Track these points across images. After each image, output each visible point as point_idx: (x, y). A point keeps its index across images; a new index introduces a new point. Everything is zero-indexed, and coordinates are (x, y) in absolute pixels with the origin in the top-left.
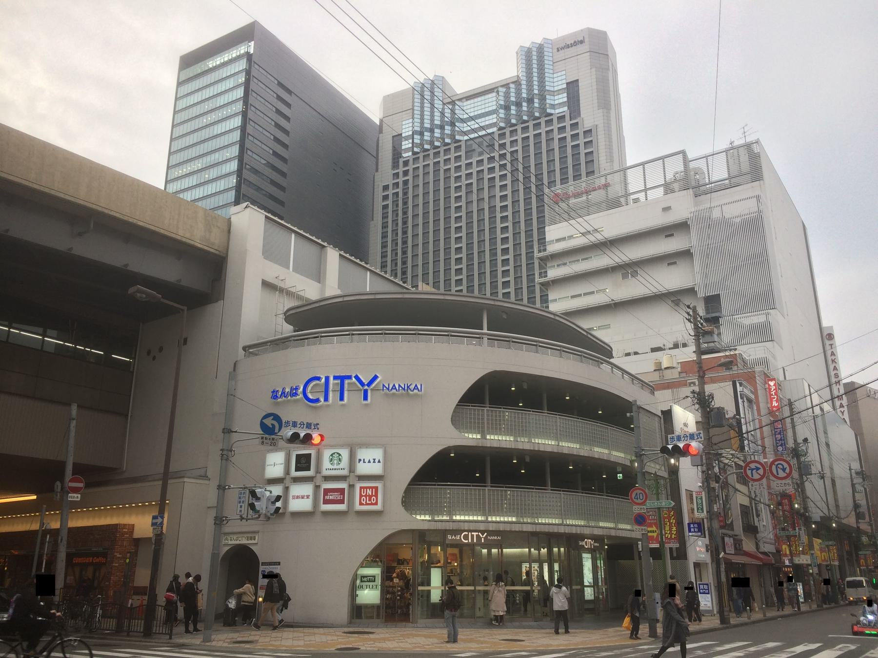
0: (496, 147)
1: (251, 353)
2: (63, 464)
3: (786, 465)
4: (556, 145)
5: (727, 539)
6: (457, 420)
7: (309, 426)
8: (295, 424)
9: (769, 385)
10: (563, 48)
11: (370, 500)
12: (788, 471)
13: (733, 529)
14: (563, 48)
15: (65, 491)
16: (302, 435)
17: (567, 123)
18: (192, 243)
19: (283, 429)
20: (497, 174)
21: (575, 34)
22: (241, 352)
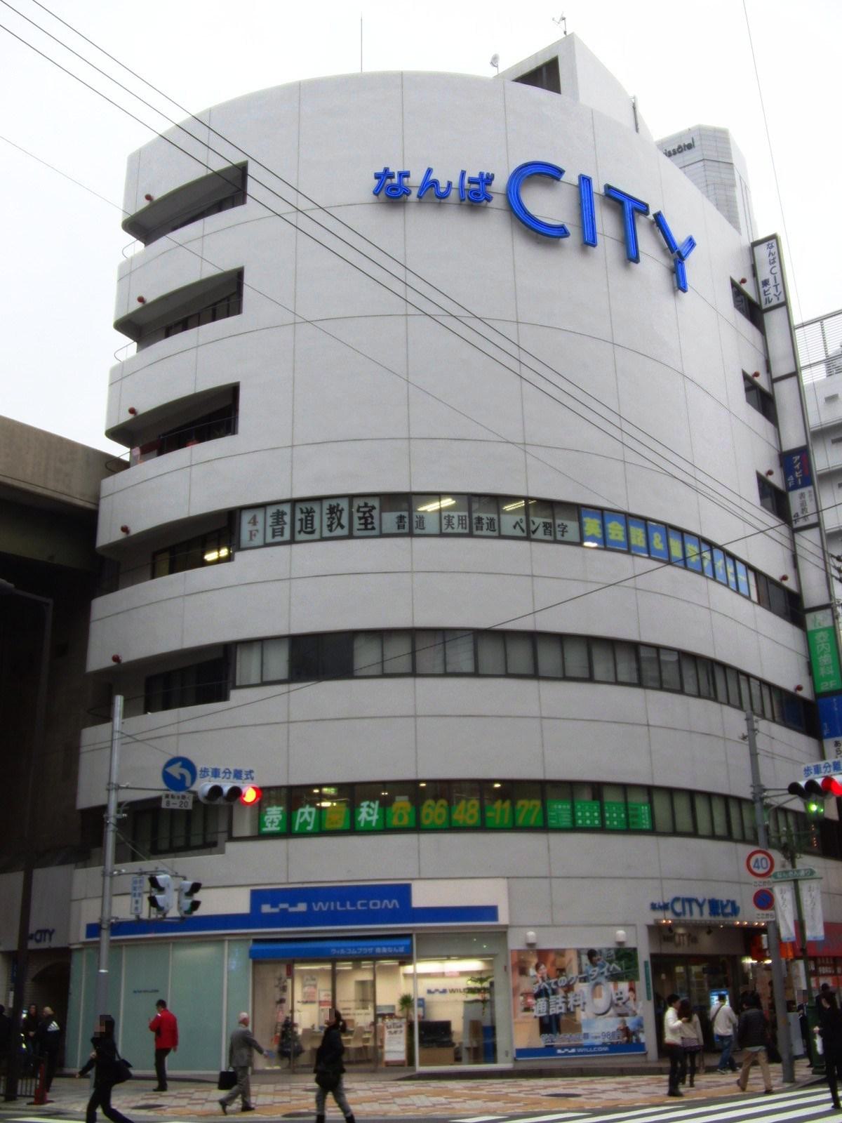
7: (238, 774)
8: (216, 773)
16: (226, 789)
19: (198, 780)
21: (680, 136)
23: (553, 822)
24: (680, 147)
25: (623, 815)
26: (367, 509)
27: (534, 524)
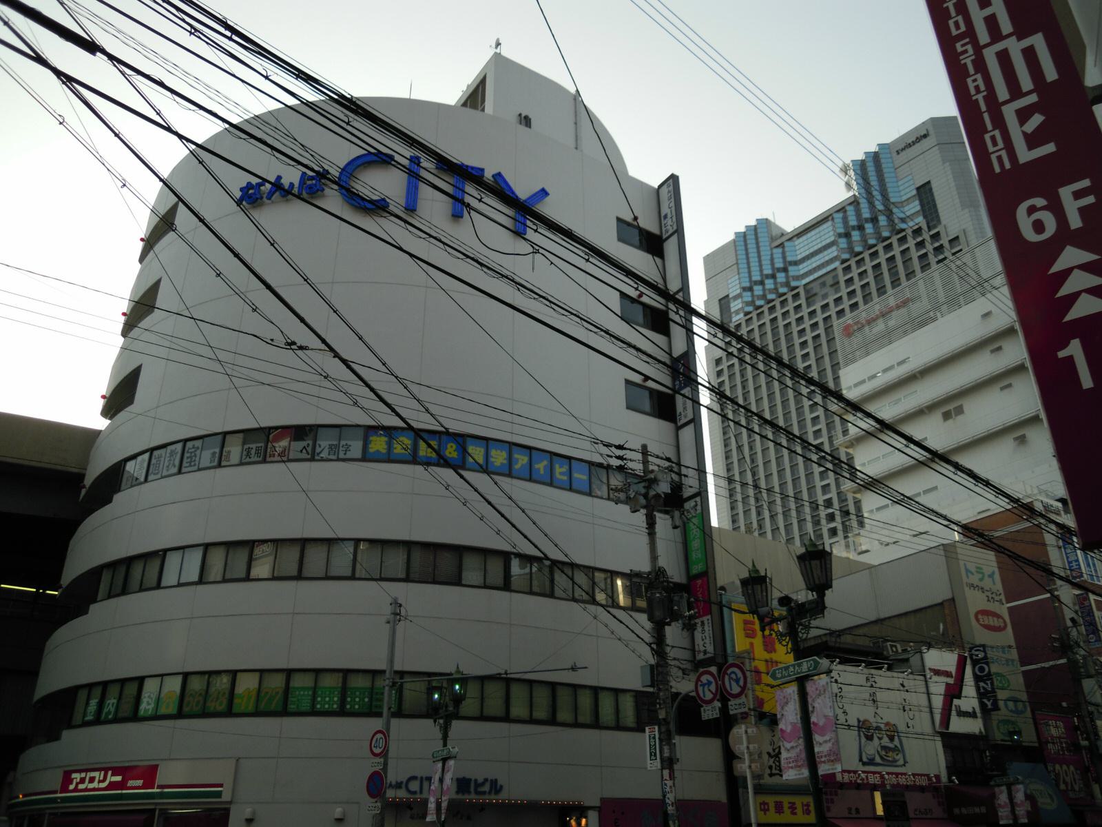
0: (842, 284)
10: (903, 149)
14: (903, 149)
21: (916, 129)
23: (292, 706)
24: (917, 138)
25: (366, 700)
26: (193, 450)
27: (320, 446)
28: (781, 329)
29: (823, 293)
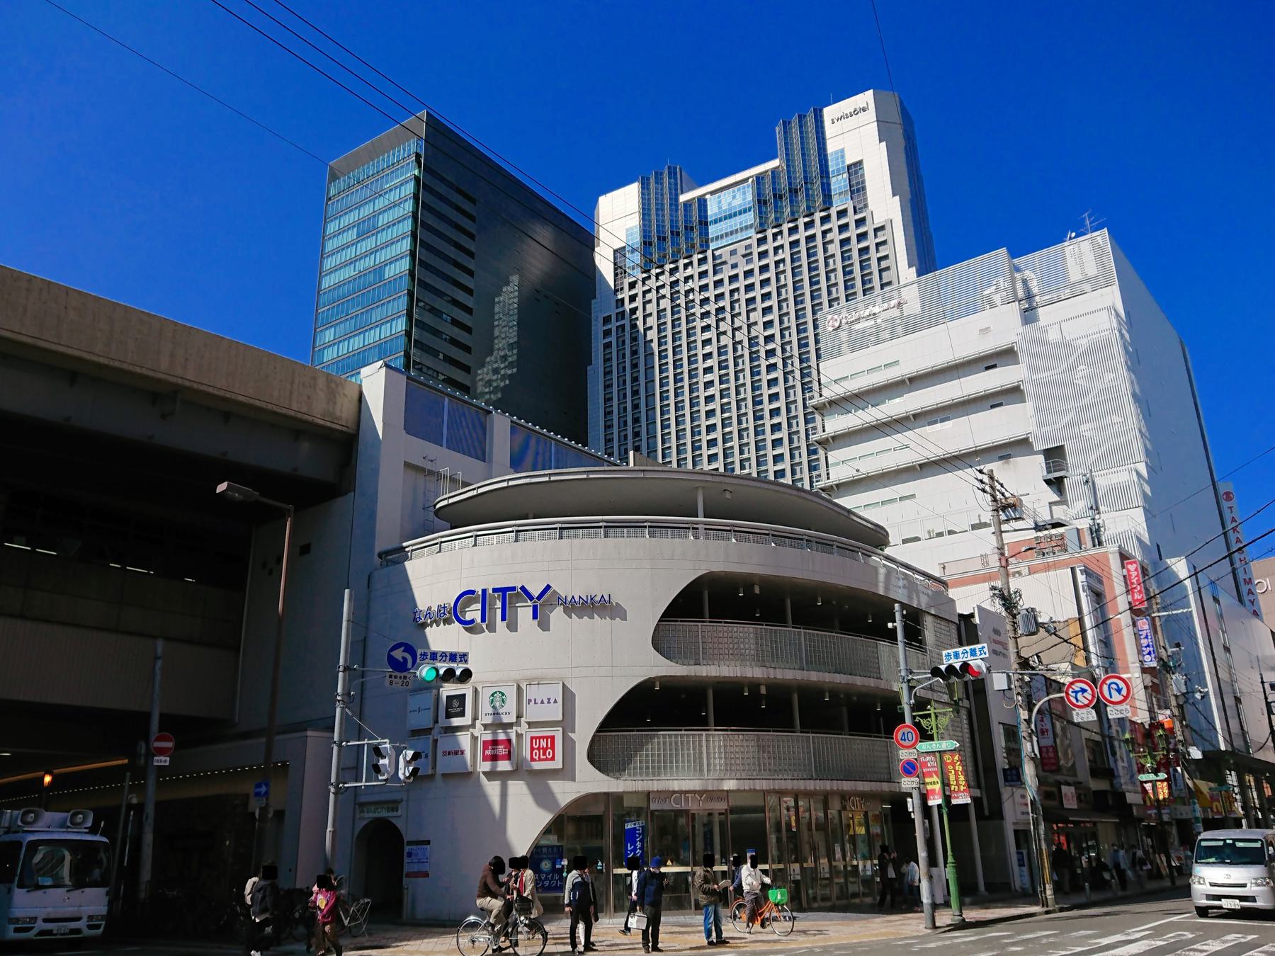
0: (755, 256)
1: (388, 561)
2: (147, 716)
3: (1121, 685)
4: (834, 249)
5: (1064, 789)
6: (658, 643)
9: (1129, 571)
11: (544, 754)
12: (1124, 692)
13: (1075, 775)
15: (150, 754)
16: (458, 673)
17: (851, 218)
18: (310, 419)
20: (757, 293)
22: (377, 560)
28: (855, 254)
29: (733, 262)
